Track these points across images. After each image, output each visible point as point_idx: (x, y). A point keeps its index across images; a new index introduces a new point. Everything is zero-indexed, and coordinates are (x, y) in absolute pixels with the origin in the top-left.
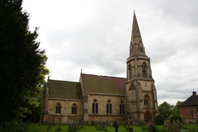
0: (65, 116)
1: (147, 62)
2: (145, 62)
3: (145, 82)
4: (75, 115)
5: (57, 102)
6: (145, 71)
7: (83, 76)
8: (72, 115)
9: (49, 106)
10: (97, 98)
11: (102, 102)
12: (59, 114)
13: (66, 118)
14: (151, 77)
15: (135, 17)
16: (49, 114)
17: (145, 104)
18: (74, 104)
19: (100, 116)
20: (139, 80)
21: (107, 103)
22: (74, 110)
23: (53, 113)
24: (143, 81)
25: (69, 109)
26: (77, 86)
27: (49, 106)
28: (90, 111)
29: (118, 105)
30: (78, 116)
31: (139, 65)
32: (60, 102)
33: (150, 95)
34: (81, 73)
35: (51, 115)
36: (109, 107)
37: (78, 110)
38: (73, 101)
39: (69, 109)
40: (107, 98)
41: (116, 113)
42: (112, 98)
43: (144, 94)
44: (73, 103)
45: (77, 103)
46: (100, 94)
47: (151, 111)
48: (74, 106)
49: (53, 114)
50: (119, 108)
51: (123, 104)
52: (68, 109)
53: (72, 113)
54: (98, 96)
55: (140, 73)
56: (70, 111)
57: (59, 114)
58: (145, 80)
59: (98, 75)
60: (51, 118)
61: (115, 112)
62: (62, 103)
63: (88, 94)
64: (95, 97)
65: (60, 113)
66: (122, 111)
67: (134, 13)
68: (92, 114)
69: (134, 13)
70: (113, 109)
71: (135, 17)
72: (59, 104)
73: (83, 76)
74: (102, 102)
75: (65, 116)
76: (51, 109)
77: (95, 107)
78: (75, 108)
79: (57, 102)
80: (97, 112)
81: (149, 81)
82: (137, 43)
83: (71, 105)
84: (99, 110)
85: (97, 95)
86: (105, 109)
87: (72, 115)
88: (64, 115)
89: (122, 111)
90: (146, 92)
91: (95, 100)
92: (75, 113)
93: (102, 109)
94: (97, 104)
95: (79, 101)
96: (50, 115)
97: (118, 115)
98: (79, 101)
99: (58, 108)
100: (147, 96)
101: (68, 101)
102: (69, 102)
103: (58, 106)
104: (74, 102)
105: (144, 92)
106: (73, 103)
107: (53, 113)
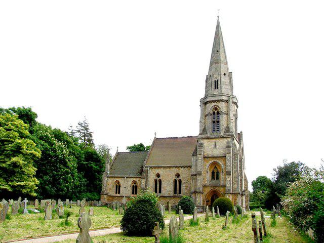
1: (222, 107)
2: (217, 106)
5: (116, 179)
6: (218, 122)
12: (118, 195)
13: (126, 199)
14: (228, 129)
15: (218, 27)
16: (109, 195)
17: (213, 178)
18: (135, 182)
23: (112, 193)
24: (211, 140)
31: (206, 113)
32: (119, 180)
33: (221, 163)
40: (176, 171)
42: (182, 169)
43: (211, 162)
44: (132, 180)
45: (137, 180)
46: (165, 166)
47: (221, 189)
48: (135, 183)
49: (112, 195)
51: (160, 178)
53: (133, 194)
57: (118, 195)
59: (179, 137)
60: (111, 199)
61: (186, 191)
62: (121, 181)
66: (158, 185)
67: (218, 20)
69: (218, 20)
70: (183, 186)
71: (218, 27)
72: (118, 182)
77: (158, 184)
78: (136, 187)
79: (116, 179)
81: (223, 137)
84: (162, 190)
85: (161, 167)
86: (171, 188)
89: (158, 185)
90: (213, 157)
91: (158, 175)
94: (160, 181)
99: (118, 188)
100: (215, 165)
101: (127, 177)
102: (128, 179)
105: (210, 159)
106: (132, 180)
107: (112, 193)
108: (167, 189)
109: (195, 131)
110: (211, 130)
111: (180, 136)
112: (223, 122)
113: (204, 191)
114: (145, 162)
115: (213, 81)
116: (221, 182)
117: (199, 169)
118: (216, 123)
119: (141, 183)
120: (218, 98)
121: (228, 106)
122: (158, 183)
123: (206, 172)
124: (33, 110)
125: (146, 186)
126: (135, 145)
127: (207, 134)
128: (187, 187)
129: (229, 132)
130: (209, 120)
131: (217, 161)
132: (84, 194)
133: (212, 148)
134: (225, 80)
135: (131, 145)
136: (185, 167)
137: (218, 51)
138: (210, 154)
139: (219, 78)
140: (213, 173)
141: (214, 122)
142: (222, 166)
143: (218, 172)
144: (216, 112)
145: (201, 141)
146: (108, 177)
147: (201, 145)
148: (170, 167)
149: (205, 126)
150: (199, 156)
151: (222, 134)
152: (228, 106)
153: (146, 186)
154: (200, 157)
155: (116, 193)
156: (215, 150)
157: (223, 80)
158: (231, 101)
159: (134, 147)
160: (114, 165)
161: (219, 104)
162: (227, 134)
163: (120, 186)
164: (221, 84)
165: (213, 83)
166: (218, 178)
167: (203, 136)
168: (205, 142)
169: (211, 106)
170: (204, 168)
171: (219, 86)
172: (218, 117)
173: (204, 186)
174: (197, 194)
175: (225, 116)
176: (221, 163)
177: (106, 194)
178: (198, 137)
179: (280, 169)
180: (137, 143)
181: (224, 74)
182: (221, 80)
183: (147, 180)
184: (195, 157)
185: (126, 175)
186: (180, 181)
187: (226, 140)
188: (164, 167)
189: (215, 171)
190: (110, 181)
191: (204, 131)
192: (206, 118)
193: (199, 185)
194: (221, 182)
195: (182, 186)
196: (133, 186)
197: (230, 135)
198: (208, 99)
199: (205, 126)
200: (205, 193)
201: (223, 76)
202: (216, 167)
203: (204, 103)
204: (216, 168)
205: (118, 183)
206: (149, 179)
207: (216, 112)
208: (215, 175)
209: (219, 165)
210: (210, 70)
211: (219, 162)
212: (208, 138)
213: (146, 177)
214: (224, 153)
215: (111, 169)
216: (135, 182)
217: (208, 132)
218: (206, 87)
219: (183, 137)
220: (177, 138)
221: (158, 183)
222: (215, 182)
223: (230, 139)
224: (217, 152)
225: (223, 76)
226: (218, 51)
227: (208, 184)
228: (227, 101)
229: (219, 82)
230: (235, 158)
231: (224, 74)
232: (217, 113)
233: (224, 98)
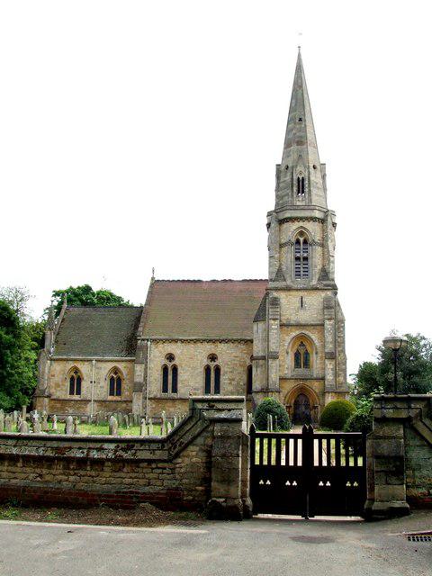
1: (313, 230)
3: (301, 293)
4: (118, 398)
5: (71, 365)
6: (306, 259)
8: (110, 398)
9: (53, 376)
10: (176, 349)
11: (191, 363)
12: (118, 398)
13: (96, 405)
14: (326, 274)
15: (299, 69)
16: (52, 397)
17: (297, 365)
18: (116, 370)
19: (183, 400)
20: (277, 289)
21: (177, 359)
22: (116, 384)
23: (63, 393)
25: (102, 384)
27: (53, 376)
28: (155, 387)
29: (241, 369)
30: (125, 401)
31: (283, 241)
33: (314, 336)
34: (153, 278)
35: (58, 400)
37: (125, 385)
38: (111, 361)
39: (102, 384)
40: (208, 348)
42: (222, 346)
43: (294, 334)
44: (110, 365)
45: (121, 366)
47: (316, 386)
48: (116, 373)
49: (63, 397)
53: (111, 394)
54: (179, 344)
55: (284, 268)
57: (76, 397)
58: (297, 290)
60: (58, 405)
61: (230, 388)
62: (84, 369)
63: (148, 340)
64: (170, 348)
65: (79, 393)
66: (170, 377)
67: (299, 55)
68: (159, 396)
69: (299, 55)
70: (224, 379)
71: (299, 69)
72: (76, 370)
73: (158, 288)
74: (191, 363)
76: (58, 385)
77: (170, 374)
78: (119, 380)
79: (71, 365)
80: (175, 390)
81: (317, 289)
83: (107, 371)
84: (179, 385)
85: (176, 341)
87: (110, 398)
89: (170, 377)
90: (299, 325)
91: (170, 357)
92: (119, 394)
94: (175, 369)
95: (126, 361)
96: (54, 400)
98: (126, 361)
99: (76, 382)
100: (302, 341)
102: (100, 365)
103: (302, 352)
106: (110, 366)
107: (63, 393)
108: (191, 384)
109: (259, 269)
110: (293, 274)
111: (206, 278)
112: (317, 260)
113: (282, 387)
114: (140, 329)
115: (295, 178)
117: (273, 347)
119: (132, 372)
121: (324, 231)
122: (170, 372)
123: (284, 353)
124: (400, 335)
125: (145, 380)
126: (71, 288)
127: (285, 280)
128: (233, 380)
129: (328, 279)
130: (288, 256)
131: (307, 332)
132: (426, 409)
134: (315, 178)
135: (64, 287)
136: (210, 341)
138: (293, 319)
139: (307, 174)
140: (297, 355)
141: (297, 259)
142: (317, 343)
143: (307, 353)
144: (302, 239)
145: (275, 294)
146: (51, 360)
147: (275, 302)
148: (196, 341)
149: (281, 264)
150: (273, 322)
151: (314, 282)
152: (324, 231)
153: (145, 380)
154: (274, 325)
155: (72, 393)
156: (302, 312)
157: (312, 178)
159: (71, 290)
160: (61, 333)
161: (309, 226)
162: (324, 282)
163: (80, 380)
164: (309, 186)
165: (295, 182)
166: (307, 364)
168: (282, 296)
169: (293, 227)
170: (283, 343)
171: (306, 190)
172: (306, 250)
173: (282, 379)
175: (319, 249)
176: (313, 337)
177: (48, 397)
179: (394, 340)
180: (77, 283)
181: (314, 167)
182: (309, 178)
183: (146, 365)
184: (261, 325)
185: (96, 354)
186: (218, 370)
188: (183, 341)
189: (302, 352)
190: (57, 367)
191: (279, 274)
192: (284, 249)
193: (274, 377)
196: (112, 379)
197: (329, 286)
198: (288, 214)
199: (281, 264)
200: (285, 391)
201: (312, 170)
202: (302, 344)
204: (304, 345)
205: (76, 372)
206: (150, 365)
207: (302, 239)
208: (302, 359)
209: (311, 342)
210: (286, 155)
211: (310, 335)
212: (288, 289)
213: (145, 361)
214: (320, 317)
215: (56, 342)
216: (116, 370)
217: (287, 276)
218: (278, 189)
219: (214, 281)
220: (199, 281)
221: (170, 372)
222: (302, 371)
224: (304, 317)
225: (312, 170)
226: (300, 120)
227: (289, 376)
228: (323, 221)
230: (339, 328)
231: (314, 167)
233: (318, 214)
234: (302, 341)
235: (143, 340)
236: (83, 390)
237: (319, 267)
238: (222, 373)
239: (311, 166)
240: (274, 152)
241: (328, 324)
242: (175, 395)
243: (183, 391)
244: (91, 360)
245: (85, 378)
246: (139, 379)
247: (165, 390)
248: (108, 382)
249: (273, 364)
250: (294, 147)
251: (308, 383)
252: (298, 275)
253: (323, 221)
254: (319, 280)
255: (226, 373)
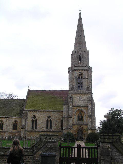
0: (6, 132)
1: (85, 73)
3: (80, 95)
4: (16, 131)
6: (82, 83)
7: (30, 92)
8: (13, 131)
10: (37, 114)
17: (78, 120)
18: (15, 121)
19: (39, 132)
20: (72, 94)
22: (15, 126)
26: (22, 103)
28: (29, 127)
31: (74, 77)
33: (84, 110)
34: (29, 89)
36: (49, 123)
37: (19, 126)
39: (10, 126)
40: (48, 114)
41: (56, 129)
42: (52, 113)
45: (17, 120)
47: (85, 127)
48: (15, 122)
50: (60, 124)
52: (9, 126)
53: (14, 129)
55: (74, 86)
56: (11, 128)
59: (46, 90)
61: (55, 128)
64: (35, 114)
66: (34, 124)
67: (80, 13)
69: (80, 13)
73: (30, 92)
75: (6, 132)
77: (34, 122)
78: (16, 124)
80: (36, 128)
81: (85, 94)
82: (76, 51)
84: (37, 127)
88: (6, 131)
89: (34, 124)
90: (79, 106)
91: (34, 117)
92: (16, 129)
93: (41, 126)
94: (36, 121)
97: (58, 131)
100: (80, 111)
102: (10, 119)
103: (80, 115)
104: (15, 119)
114: (24, 107)
116: (85, 122)
117: (70, 113)
118: (81, 84)
120: (82, 68)
127: (74, 91)
130: (75, 82)
131: (82, 109)
133: (78, 100)
137: (80, 36)
140: (78, 116)
142: (85, 112)
143: (82, 116)
144: (80, 77)
147: (71, 98)
151: (85, 92)
158: (89, 70)
166: (82, 120)
167: (72, 92)
169: (77, 73)
170: (74, 113)
173: (73, 125)
174: (69, 130)
178: (70, 92)
182: (83, 56)
184: (66, 106)
186: (51, 121)
187: (87, 96)
188: (39, 111)
189: (80, 115)
191: (72, 87)
193: (70, 124)
194: (85, 122)
195: (52, 124)
196: (14, 124)
198: (75, 68)
201: (84, 53)
203: (71, 70)
207: (80, 77)
208: (80, 118)
212: (76, 94)
216: (15, 121)
222: (80, 122)
223: (90, 95)
224: (81, 103)
226: (80, 36)
229: (78, 60)
232: (80, 77)
233: (85, 68)
234: (80, 111)
235: (25, 111)
236: (4, 128)
237: (87, 86)
238: (52, 122)
239: (84, 51)
240: (71, 46)
241: (89, 106)
242: (36, 130)
243: (39, 128)
244: (7, 118)
245: (5, 124)
246: (23, 124)
247: (33, 128)
248: (12, 125)
249: (70, 120)
250: (78, 45)
251: (82, 126)
252: (79, 89)
253: (88, 70)
254: (86, 91)
255: (54, 122)
